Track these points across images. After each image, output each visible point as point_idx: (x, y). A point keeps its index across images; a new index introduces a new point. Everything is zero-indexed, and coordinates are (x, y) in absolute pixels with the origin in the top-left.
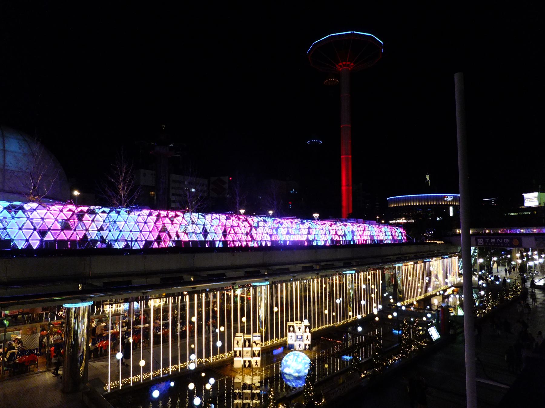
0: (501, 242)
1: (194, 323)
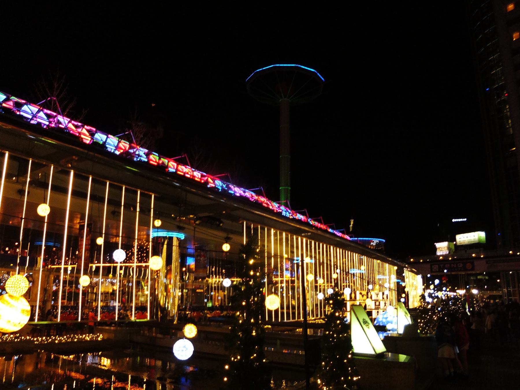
0: (455, 266)
1: (213, 271)
